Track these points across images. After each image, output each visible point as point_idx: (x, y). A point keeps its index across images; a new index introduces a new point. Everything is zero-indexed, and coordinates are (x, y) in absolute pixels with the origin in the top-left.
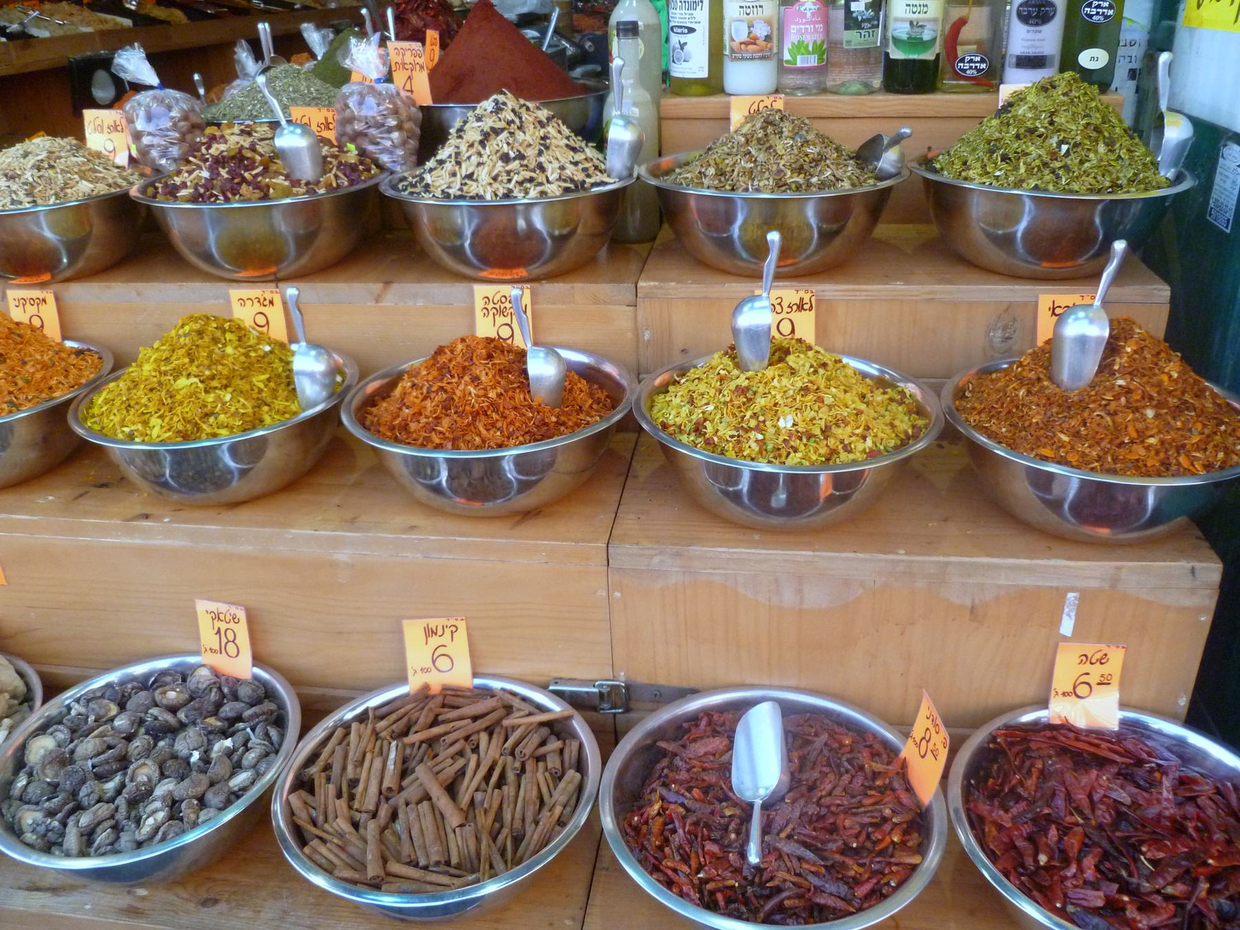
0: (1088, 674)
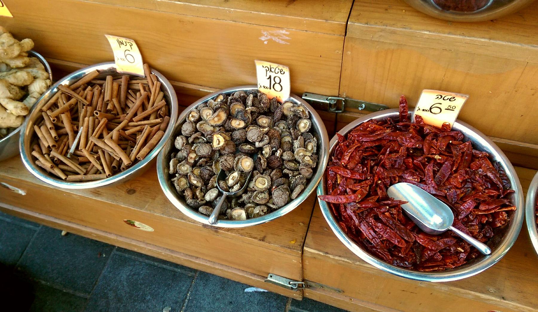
0: (441, 104)
